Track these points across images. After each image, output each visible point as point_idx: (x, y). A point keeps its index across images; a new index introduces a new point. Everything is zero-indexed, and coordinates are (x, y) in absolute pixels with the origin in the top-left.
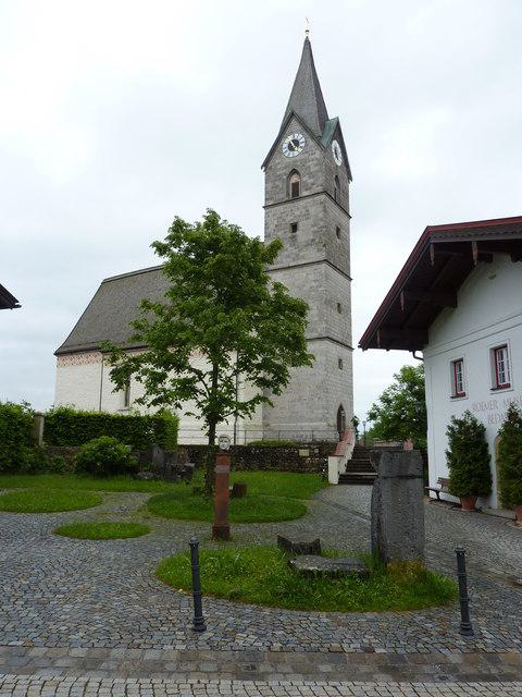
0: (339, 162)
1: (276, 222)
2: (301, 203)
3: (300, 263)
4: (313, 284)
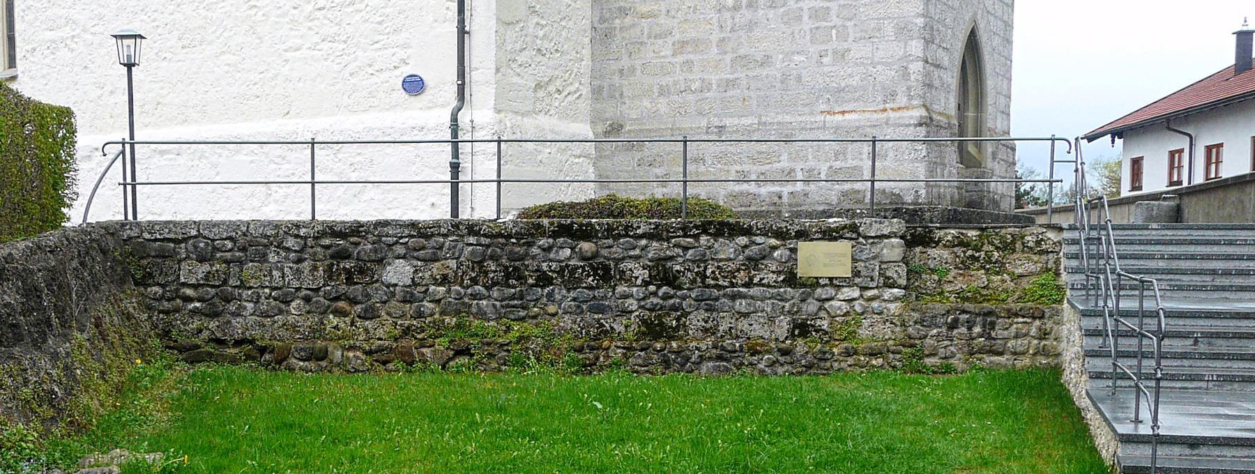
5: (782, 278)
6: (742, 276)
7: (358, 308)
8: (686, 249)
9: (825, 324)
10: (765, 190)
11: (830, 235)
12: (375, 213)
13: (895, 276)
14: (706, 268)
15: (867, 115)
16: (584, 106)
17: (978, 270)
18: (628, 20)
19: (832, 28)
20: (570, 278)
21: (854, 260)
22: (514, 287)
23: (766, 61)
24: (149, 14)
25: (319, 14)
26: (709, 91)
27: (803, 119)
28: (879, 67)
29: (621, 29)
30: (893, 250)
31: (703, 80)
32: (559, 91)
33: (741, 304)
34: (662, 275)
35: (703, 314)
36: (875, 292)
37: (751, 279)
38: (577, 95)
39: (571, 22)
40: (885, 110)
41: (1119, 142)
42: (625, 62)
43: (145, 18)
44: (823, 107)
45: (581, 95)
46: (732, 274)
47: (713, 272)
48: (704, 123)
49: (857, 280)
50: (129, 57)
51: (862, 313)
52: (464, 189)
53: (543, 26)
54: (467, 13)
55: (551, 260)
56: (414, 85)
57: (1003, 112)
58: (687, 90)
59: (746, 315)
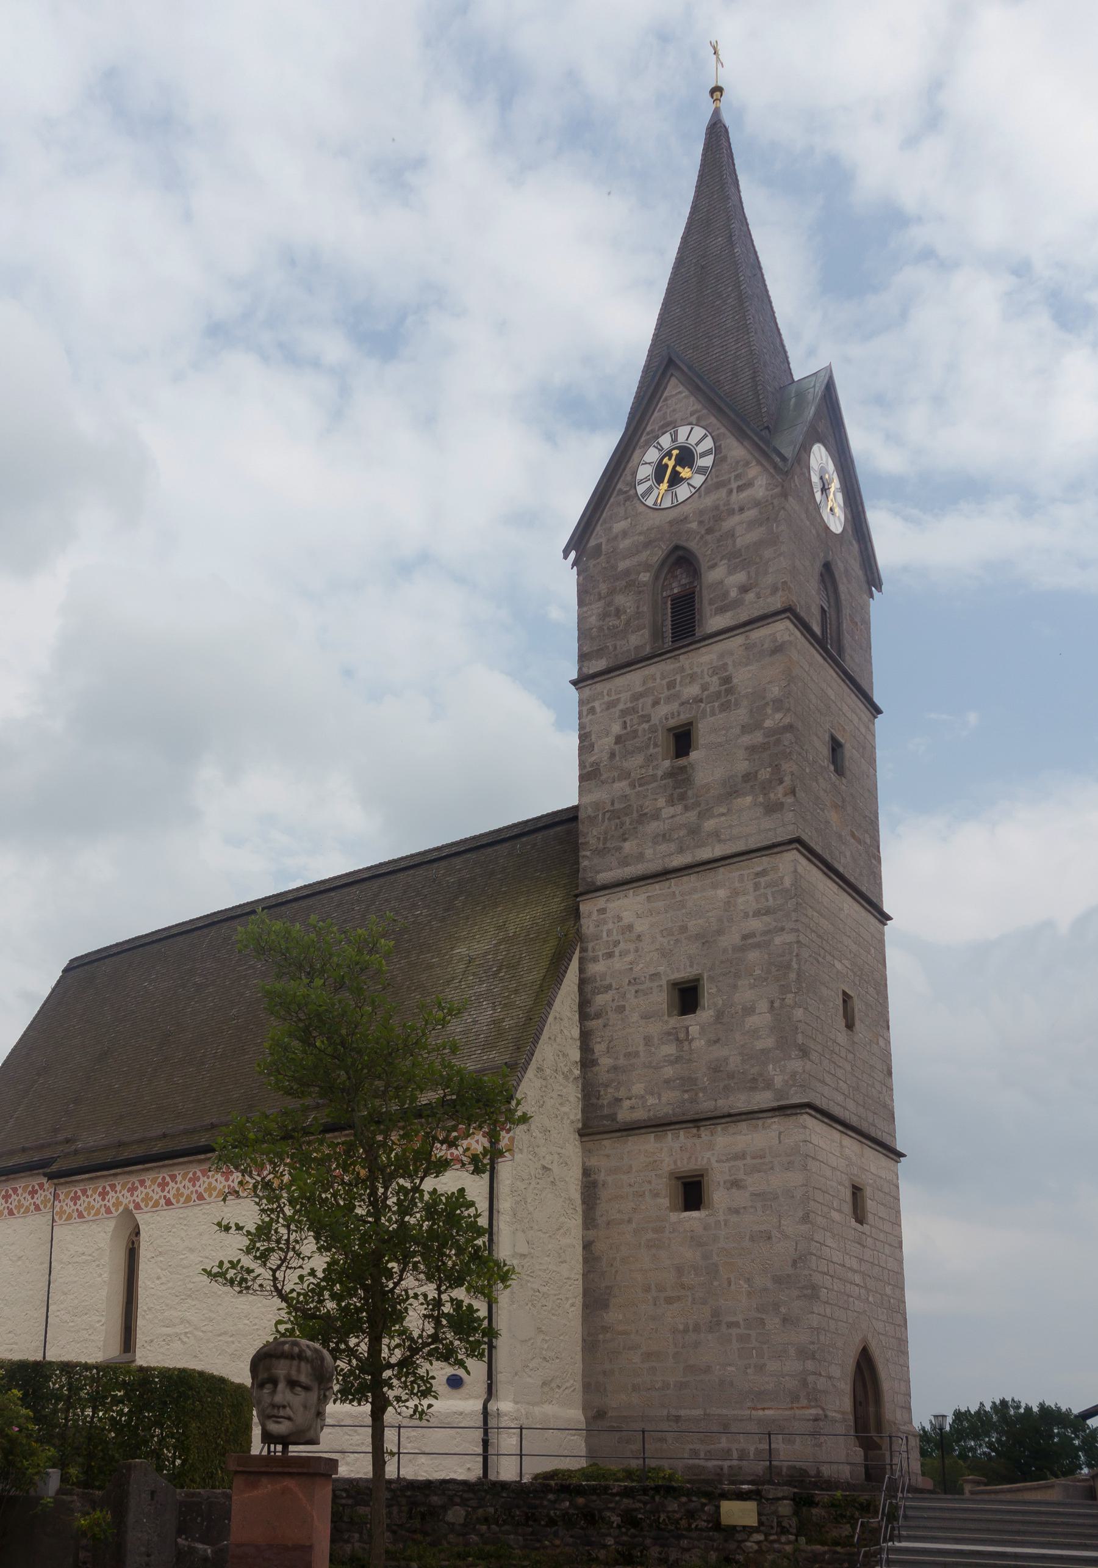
0: (836, 521)
1: (616, 729)
2: (704, 658)
5: (710, 1525)
7: (428, 1539)
8: (645, 1504)
10: (710, 1464)
11: (741, 1496)
12: (425, 1474)
13: (788, 1526)
14: (659, 1517)
15: (780, 1412)
16: (578, 1397)
17: (846, 1523)
18: (608, 1335)
19: (753, 1348)
21: (759, 1514)
22: (531, 1526)
23: (708, 1370)
24: (250, 1320)
26: (668, 1389)
27: (736, 1412)
28: (787, 1378)
29: (603, 1341)
30: (785, 1508)
32: (559, 1387)
33: (684, 1542)
34: (630, 1520)
35: (658, 1549)
37: (690, 1525)
38: (572, 1389)
39: (567, 1337)
40: (792, 1408)
43: (247, 1322)
44: (749, 1404)
45: (575, 1389)
46: (677, 1522)
47: (664, 1520)
48: (665, 1413)
49: (762, 1528)
51: (767, 1551)
52: (492, 1460)
53: (547, 1341)
55: (556, 1509)
57: (902, 1407)
59: (688, 1550)
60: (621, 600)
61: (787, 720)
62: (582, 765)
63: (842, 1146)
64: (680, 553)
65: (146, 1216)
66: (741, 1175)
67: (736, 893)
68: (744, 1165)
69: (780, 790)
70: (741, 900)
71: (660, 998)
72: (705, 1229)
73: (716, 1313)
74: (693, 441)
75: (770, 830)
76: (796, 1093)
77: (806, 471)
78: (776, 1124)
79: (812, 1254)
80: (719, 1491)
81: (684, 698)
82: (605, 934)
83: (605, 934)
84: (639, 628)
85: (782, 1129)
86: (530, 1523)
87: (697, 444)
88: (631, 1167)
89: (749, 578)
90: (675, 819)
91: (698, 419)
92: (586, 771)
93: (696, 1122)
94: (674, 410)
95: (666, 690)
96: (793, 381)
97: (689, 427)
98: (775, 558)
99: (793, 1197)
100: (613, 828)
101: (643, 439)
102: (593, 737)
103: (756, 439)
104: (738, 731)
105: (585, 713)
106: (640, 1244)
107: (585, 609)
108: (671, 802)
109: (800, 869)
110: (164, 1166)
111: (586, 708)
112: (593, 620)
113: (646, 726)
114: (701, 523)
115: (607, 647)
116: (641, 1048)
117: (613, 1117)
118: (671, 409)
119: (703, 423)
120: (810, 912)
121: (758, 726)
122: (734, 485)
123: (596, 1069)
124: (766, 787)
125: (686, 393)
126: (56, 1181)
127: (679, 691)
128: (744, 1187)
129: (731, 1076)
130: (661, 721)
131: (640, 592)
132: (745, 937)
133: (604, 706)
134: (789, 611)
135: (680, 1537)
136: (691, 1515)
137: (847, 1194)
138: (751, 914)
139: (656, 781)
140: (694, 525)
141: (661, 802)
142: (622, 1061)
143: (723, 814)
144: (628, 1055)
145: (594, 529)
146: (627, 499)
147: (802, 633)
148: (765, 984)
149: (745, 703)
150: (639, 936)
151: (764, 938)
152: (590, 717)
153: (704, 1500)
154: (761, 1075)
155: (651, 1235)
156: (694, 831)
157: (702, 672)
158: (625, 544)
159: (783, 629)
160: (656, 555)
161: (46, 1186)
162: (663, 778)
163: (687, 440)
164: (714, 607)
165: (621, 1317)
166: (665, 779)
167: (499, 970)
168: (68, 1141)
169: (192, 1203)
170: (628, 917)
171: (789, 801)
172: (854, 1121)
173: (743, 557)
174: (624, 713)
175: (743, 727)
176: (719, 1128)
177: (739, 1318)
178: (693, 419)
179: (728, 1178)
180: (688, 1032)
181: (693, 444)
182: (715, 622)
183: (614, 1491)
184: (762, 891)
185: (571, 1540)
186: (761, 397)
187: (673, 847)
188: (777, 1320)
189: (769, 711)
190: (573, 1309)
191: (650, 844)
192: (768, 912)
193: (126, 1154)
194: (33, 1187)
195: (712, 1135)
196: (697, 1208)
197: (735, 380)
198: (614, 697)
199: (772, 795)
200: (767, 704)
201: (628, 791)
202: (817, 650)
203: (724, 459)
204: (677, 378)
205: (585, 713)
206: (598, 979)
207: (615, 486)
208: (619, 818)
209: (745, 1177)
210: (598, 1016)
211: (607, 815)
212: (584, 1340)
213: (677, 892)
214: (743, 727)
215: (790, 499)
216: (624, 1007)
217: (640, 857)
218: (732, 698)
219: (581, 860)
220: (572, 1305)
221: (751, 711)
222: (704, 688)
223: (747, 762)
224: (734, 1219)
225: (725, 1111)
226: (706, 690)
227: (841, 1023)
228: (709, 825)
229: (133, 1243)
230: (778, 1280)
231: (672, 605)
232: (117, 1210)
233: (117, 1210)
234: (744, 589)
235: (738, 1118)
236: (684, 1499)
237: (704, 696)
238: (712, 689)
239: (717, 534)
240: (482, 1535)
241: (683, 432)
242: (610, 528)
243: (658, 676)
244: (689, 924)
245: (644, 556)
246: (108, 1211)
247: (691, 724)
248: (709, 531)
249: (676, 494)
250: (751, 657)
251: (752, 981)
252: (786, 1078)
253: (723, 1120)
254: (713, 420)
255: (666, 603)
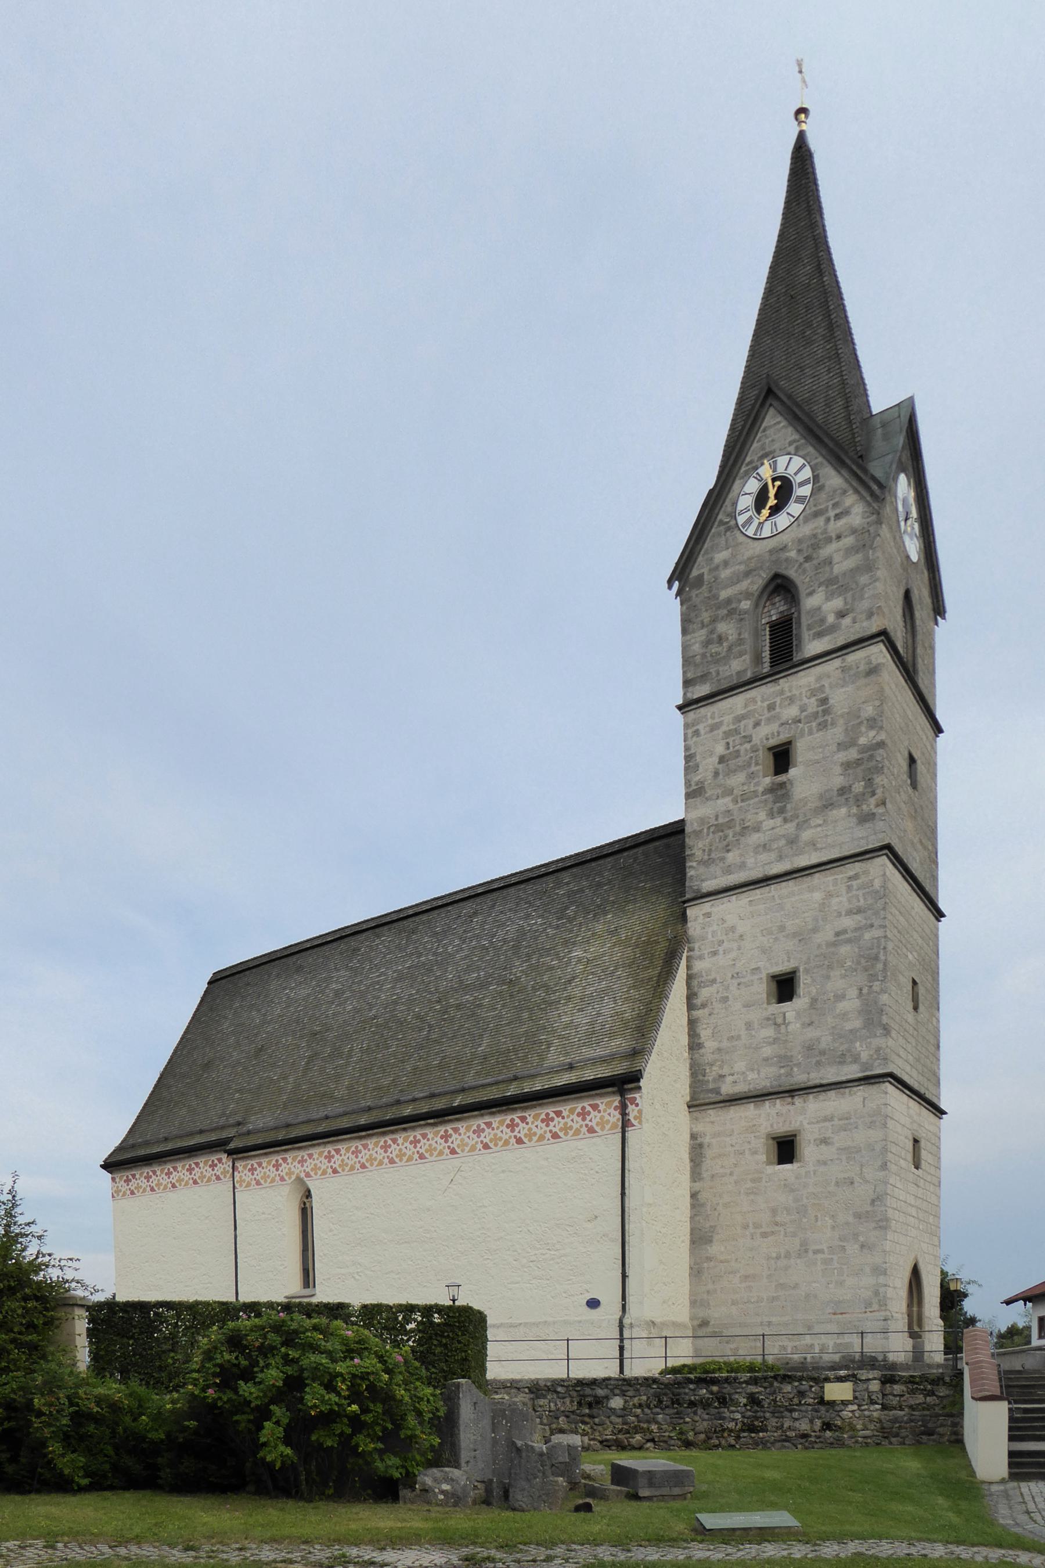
1: (720, 749)
2: (802, 682)
3: (803, 861)
4: (848, 922)
6: (796, 1401)
9: (839, 1423)
18: (712, 1264)
20: (705, 1404)
21: (854, 1391)
23: (796, 1286)
25: (531, 1264)
30: (875, 1386)
31: (758, 1297)
36: (866, 1407)
37: (800, 1402)
41: (1029, 1305)
42: (710, 1287)
46: (791, 1400)
49: (856, 1401)
50: (453, 1296)
54: (627, 1266)
56: (593, 1304)
58: (749, 1302)
59: (797, 1419)
60: (722, 627)
61: (879, 738)
62: (688, 783)
63: (908, 1108)
64: (779, 581)
65: (316, 1182)
66: (829, 1134)
67: (830, 895)
68: (832, 1125)
69: (873, 801)
70: (835, 901)
71: (761, 988)
72: (797, 1178)
73: (804, 1244)
74: (792, 470)
75: (862, 838)
76: (880, 1064)
77: (894, 500)
78: (861, 1092)
79: (887, 1194)
80: (823, 1377)
81: (784, 718)
82: (710, 936)
83: (710, 936)
84: (741, 654)
85: (866, 1095)
86: (675, 1406)
87: (796, 474)
88: (733, 1131)
89: (846, 603)
90: (775, 830)
91: (797, 449)
92: (691, 789)
93: (792, 1092)
94: (773, 441)
95: (766, 711)
96: (872, 416)
97: (788, 457)
98: (870, 584)
99: (874, 1150)
100: (717, 840)
101: (743, 469)
102: (698, 758)
103: (854, 467)
104: (834, 748)
105: (690, 735)
106: (740, 1192)
107: (688, 637)
108: (771, 815)
109: (888, 873)
110: (329, 1142)
111: (691, 731)
112: (697, 648)
113: (748, 746)
114: (799, 551)
115: (710, 673)
116: (743, 1033)
117: (717, 1091)
118: (770, 439)
119: (801, 453)
120: (894, 910)
121: (852, 743)
122: (832, 514)
123: (702, 1051)
124: (859, 800)
125: (784, 423)
126: (235, 1156)
127: (779, 713)
128: (832, 1144)
129: (823, 1053)
130: (762, 742)
131: (742, 620)
132: (837, 934)
133: (708, 729)
134: (883, 635)
135: (791, 1411)
136: (801, 1394)
137: (910, 1145)
138: (843, 913)
139: (758, 796)
140: (793, 554)
141: (762, 815)
142: (725, 1044)
143: (820, 825)
144: (731, 1038)
145: (696, 558)
146: (729, 529)
147: (892, 657)
148: (855, 973)
149: (841, 721)
150: (741, 936)
151: (855, 934)
152: (695, 739)
153: (811, 1383)
154: (849, 1051)
155: (749, 1185)
156: (792, 841)
157: (801, 694)
158: (725, 574)
159: (878, 652)
160: (756, 583)
161: (224, 1160)
162: (764, 793)
163: (786, 470)
164: (812, 632)
165: (723, 1249)
166: (766, 794)
167: (616, 969)
168: (239, 1124)
169: (355, 1171)
170: (731, 920)
171: (880, 811)
172: (916, 1086)
173: (840, 584)
174: (727, 734)
175: (839, 744)
176: (811, 1096)
177: (824, 1247)
178: (792, 449)
179: (817, 1136)
180: (785, 1017)
181: (792, 474)
182: (812, 647)
183: (742, 1380)
184: (854, 892)
185: (706, 1417)
186: (854, 426)
187: (773, 855)
188: (856, 1246)
189: (863, 729)
190: (683, 1244)
191: (752, 854)
192: (859, 911)
193: (294, 1133)
194: (213, 1161)
195: (805, 1102)
196: (791, 1162)
197: (828, 410)
198: (717, 720)
199: (864, 807)
200: (862, 722)
201: (731, 806)
202: (900, 672)
203: (821, 488)
204: (776, 409)
205: (690, 735)
206: (704, 974)
207: (716, 518)
208: (722, 831)
209: (832, 1135)
210: (704, 1006)
211: (712, 830)
212: (691, 1268)
213: (776, 896)
214: (839, 744)
215: (884, 526)
216: (727, 997)
217: (742, 866)
218: (829, 718)
219: (687, 870)
220: (683, 1242)
221: (846, 729)
222: (803, 709)
223: (842, 777)
224: (822, 1169)
225: (817, 1082)
226: (805, 711)
227: (910, 1005)
228: (806, 835)
229: (305, 1203)
230: (858, 1216)
231: (770, 631)
232: (290, 1178)
233: (290, 1178)
234: (841, 615)
235: (829, 1088)
236: (796, 1384)
237: (802, 717)
238: (810, 710)
239: (815, 562)
240: (637, 1416)
241: (782, 461)
242: (712, 559)
243: (759, 699)
244: (787, 924)
245: (744, 585)
246: (282, 1179)
247: (790, 743)
248: (808, 559)
249: (775, 524)
250: (847, 679)
251: (844, 972)
252: (871, 1053)
253: (815, 1090)
254: (810, 449)
255: (765, 629)
